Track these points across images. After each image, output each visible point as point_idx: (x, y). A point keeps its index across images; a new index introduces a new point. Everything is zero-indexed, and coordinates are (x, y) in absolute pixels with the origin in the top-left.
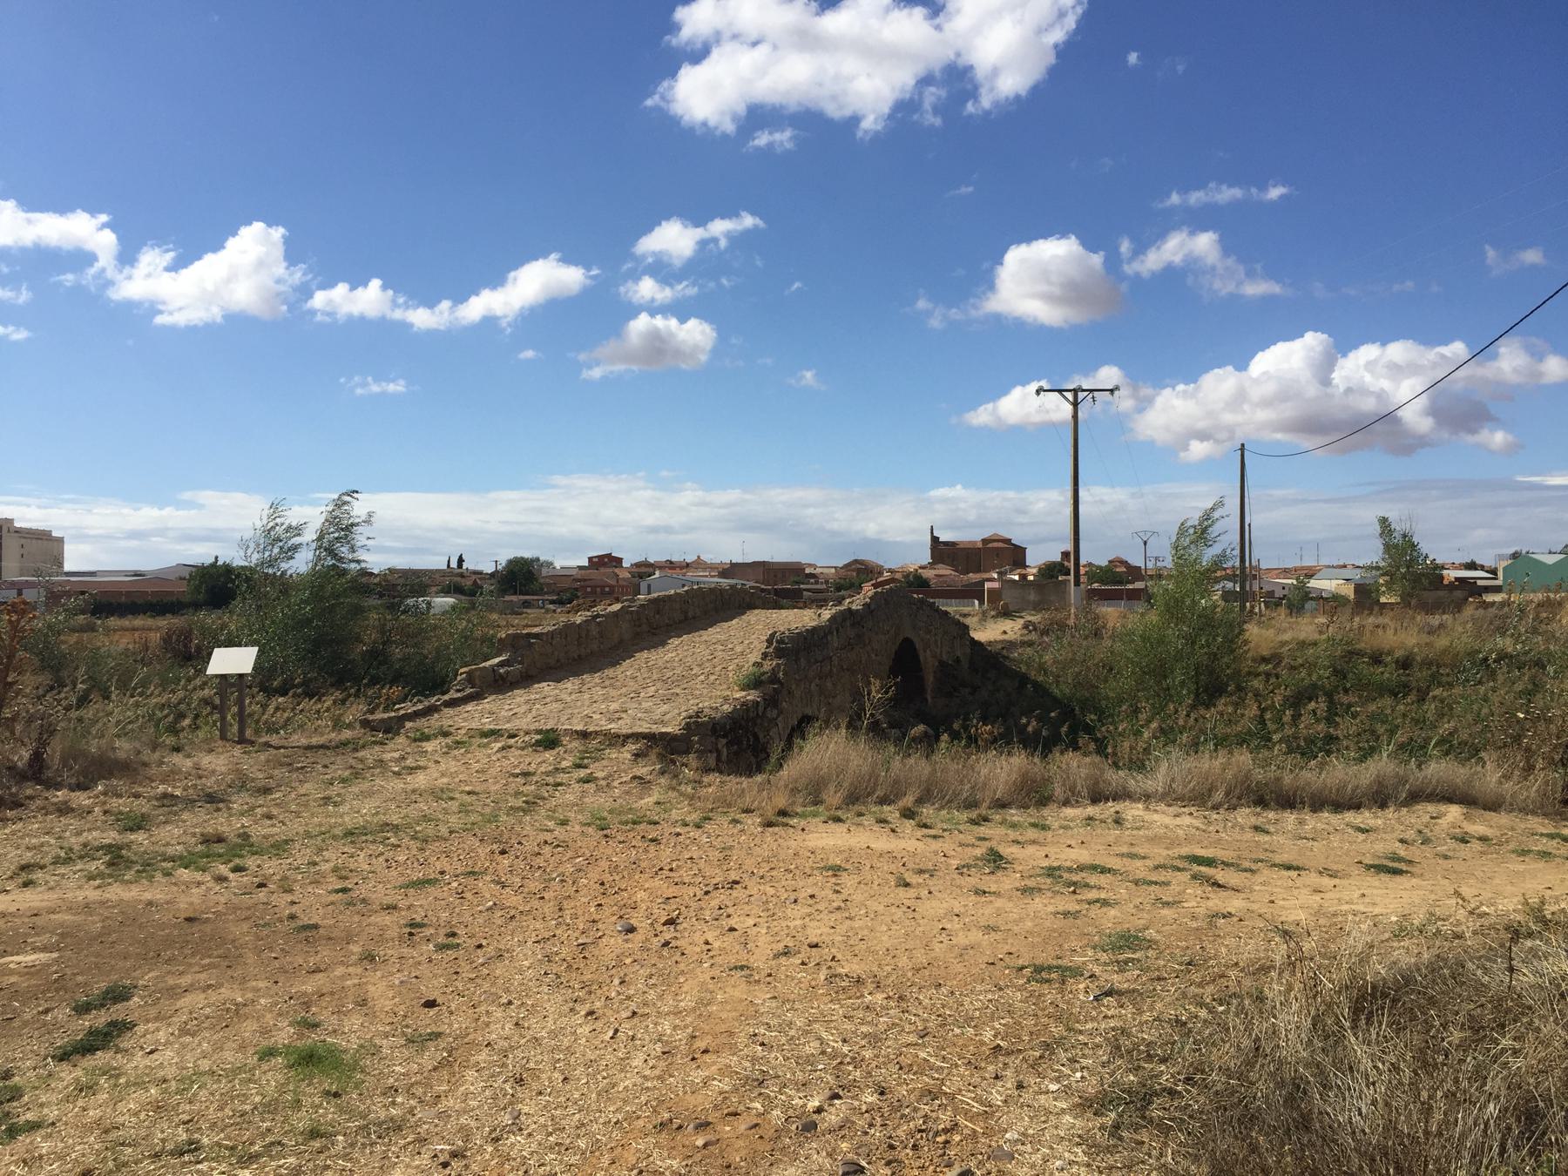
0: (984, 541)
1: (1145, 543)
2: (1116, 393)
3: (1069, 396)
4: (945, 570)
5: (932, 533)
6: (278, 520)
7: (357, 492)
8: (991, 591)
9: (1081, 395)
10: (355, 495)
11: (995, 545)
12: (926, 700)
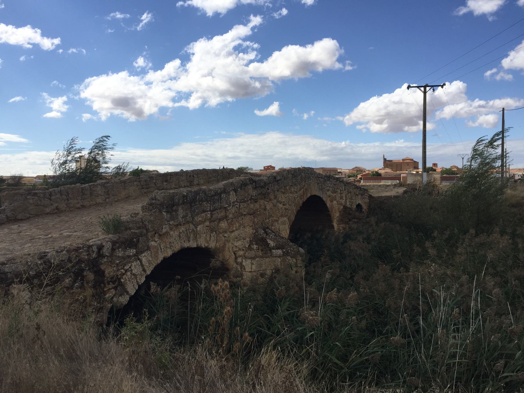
0: (403, 160)
1: (463, 158)
2: (444, 87)
3: (422, 89)
4: (388, 170)
5: (384, 157)
6: (73, 145)
7: (109, 137)
8: (403, 177)
9: (428, 88)
10: (109, 138)
11: (407, 161)
12: (333, 227)
